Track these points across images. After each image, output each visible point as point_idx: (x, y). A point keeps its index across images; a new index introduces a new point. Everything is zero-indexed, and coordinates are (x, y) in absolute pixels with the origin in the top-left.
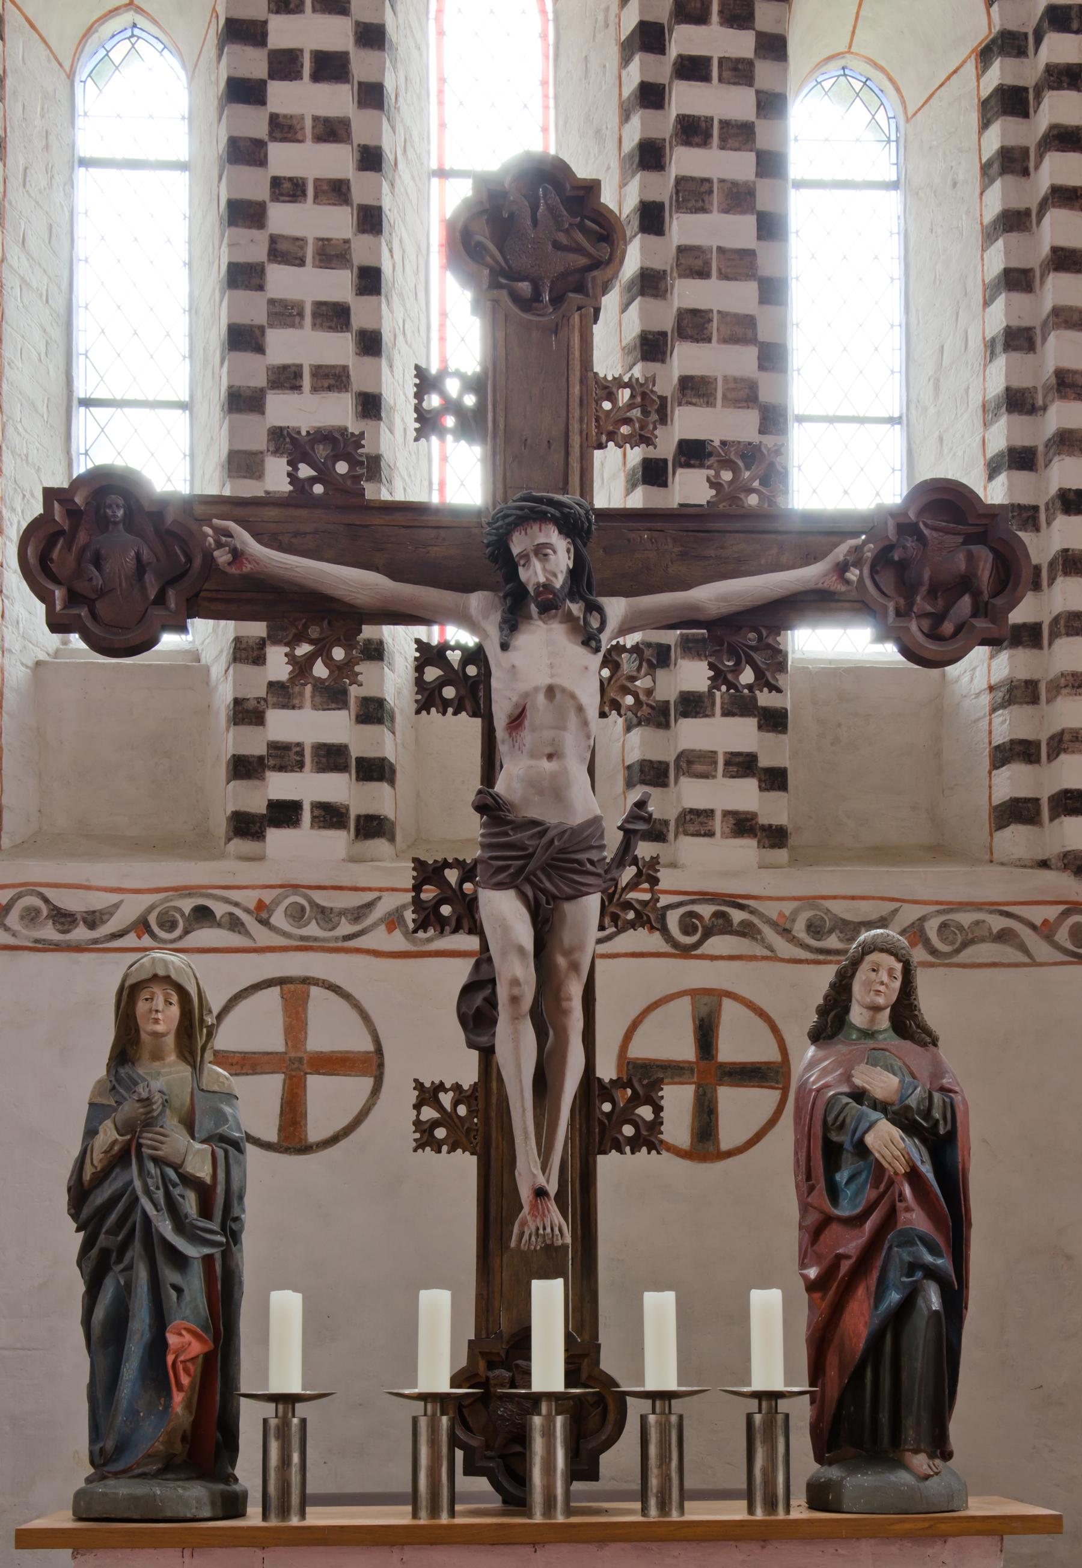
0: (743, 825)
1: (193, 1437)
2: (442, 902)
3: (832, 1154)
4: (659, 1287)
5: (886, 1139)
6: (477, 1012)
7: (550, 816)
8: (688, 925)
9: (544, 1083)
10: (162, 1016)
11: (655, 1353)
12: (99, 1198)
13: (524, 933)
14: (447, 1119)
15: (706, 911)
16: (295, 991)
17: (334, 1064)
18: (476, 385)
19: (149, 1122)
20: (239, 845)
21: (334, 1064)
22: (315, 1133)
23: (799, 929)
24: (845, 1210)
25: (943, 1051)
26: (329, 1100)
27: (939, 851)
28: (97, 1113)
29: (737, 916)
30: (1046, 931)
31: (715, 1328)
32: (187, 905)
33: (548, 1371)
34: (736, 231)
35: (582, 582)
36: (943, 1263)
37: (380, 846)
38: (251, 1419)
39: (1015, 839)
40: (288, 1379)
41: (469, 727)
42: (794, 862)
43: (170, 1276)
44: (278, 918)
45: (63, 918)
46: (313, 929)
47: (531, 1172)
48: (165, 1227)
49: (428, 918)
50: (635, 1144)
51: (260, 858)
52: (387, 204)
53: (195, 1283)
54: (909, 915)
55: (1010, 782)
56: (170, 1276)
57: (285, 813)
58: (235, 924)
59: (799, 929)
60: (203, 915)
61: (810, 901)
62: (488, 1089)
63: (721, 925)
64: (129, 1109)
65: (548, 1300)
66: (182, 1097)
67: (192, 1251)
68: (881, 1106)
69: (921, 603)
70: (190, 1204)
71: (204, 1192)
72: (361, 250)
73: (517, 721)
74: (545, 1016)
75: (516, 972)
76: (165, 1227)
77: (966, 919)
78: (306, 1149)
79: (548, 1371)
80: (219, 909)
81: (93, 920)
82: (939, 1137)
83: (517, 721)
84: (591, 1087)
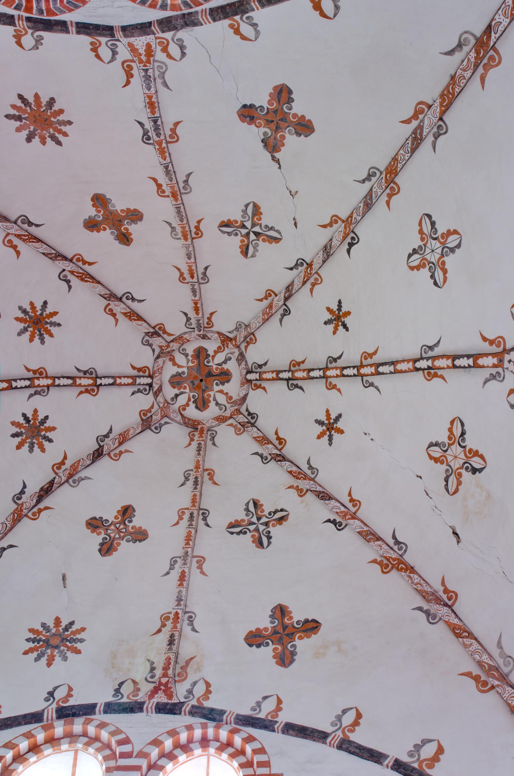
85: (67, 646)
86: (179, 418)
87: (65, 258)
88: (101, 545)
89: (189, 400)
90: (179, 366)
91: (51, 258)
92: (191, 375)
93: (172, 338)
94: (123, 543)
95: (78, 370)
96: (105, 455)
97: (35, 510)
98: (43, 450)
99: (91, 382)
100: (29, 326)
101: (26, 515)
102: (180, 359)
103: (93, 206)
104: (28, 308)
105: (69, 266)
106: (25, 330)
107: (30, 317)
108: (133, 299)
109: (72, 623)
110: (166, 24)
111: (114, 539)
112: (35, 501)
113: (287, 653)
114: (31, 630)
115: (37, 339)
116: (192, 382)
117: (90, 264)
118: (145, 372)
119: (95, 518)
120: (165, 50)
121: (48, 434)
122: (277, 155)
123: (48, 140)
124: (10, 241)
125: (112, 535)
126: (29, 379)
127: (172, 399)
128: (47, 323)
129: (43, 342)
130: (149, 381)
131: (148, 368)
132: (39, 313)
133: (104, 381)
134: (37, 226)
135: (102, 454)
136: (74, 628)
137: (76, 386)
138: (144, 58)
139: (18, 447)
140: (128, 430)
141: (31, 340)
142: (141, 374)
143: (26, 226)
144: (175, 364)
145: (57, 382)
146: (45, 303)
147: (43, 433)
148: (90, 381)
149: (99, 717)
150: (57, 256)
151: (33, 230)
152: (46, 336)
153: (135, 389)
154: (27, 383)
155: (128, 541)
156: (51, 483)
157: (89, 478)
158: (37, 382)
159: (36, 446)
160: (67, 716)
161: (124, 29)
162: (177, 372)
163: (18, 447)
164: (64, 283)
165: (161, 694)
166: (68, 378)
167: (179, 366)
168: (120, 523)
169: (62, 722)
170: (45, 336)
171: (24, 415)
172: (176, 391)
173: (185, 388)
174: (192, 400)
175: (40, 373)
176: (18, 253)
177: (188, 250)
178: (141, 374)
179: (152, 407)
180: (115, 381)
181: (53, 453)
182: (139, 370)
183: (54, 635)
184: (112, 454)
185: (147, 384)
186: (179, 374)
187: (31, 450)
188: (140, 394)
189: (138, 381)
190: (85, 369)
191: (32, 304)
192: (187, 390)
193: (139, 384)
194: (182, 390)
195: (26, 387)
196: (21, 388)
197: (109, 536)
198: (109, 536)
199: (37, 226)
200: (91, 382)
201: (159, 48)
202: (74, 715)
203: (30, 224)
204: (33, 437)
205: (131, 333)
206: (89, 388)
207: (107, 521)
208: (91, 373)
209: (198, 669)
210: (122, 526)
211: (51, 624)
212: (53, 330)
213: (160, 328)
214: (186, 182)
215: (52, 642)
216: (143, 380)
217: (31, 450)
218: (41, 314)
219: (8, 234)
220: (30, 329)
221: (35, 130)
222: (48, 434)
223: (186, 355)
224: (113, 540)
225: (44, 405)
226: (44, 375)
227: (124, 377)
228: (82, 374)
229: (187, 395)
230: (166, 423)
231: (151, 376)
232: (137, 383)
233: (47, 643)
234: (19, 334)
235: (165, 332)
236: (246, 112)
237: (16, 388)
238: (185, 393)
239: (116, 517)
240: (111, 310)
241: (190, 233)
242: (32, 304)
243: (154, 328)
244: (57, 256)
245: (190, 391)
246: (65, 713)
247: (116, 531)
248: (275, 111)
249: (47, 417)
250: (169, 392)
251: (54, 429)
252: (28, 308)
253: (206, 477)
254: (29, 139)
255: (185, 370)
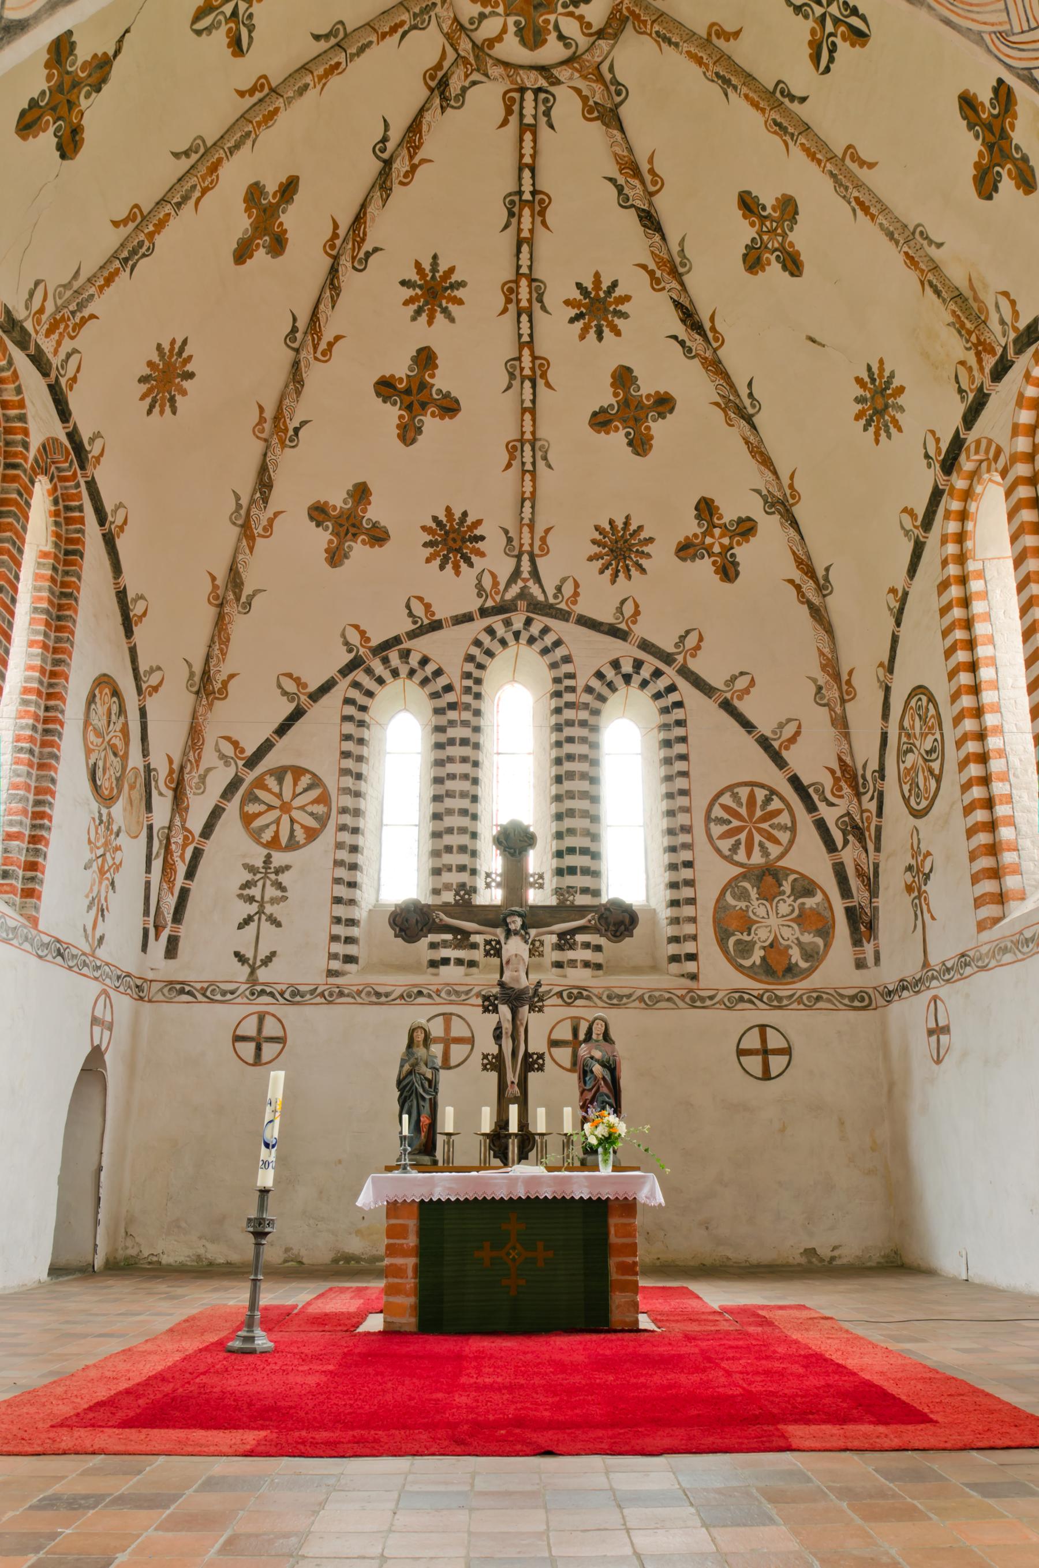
0: (587, 964)
1: (426, 1145)
2: (489, 1005)
3: (585, 1073)
4: (486, 1105)
5: (597, 1069)
6: (498, 1036)
7: (516, 986)
8: (570, 996)
9: (514, 1054)
10: (420, 1036)
11: (540, 1123)
12: (404, 1083)
13: (509, 1016)
14: (490, 1063)
15: (575, 991)
16: (447, 1017)
17: (459, 1040)
18: (500, 875)
19: (417, 1064)
20: (432, 970)
21: (459, 1040)
22: (453, 1063)
23: (604, 997)
24: (588, 1087)
25: (617, 1046)
26: (458, 1052)
27: (654, 969)
28: (403, 1062)
29: (585, 993)
30: (682, 998)
31: (554, 1117)
32: (415, 990)
33: (513, 1127)
34: (584, 785)
35: (524, 926)
36: (612, 1101)
37: (474, 970)
38: (440, 1140)
39: (674, 967)
40: (449, 1128)
41: (497, 960)
42: (605, 974)
43: (422, 1103)
44: (443, 994)
45: (378, 994)
46: (453, 998)
47: (511, 1077)
48: (421, 1091)
49: (486, 1010)
50: (538, 1070)
51: (437, 975)
52: (478, 848)
53: (427, 1105)
54: (639, 992)
55: (673, 949)
56: (422, 1103)
57: (445, 961)
58: (430, 996)
59: (604, 997)
60: (420, 993)
61: (608, 988)
62: (500, 1057)
63: (580, 996)
64: (412, 1060)
65: (513, 1110)
66: (425, 1057)
67: (427, 1097)
68: (597, 1061)
69: (612, 928)
70: (426, 1084)
71: (430, 1082)
72: (475, 689)
73: (508, 962)
74: (514, 1037)
75: (507, 1026)
76: (421, 1091)
77: (657, 994)
78: (450, 1068)
79: (513, 1127)
80: (425, 991)
81: (387, 995)
82: (611, 1067)
83: (508, 962)
84: (527, 1055)
85: (890, 396)
86: (603, 44)
87: (334, 271)
88: (785, 268)
89: (571, 14)
90: (504, 30)
91: (338, 295)
92: (522, 9)
93: (449, 50)
94: (792, 237)
95: (506, 227)
96: (651, 204)
97: (710, 335)
98: (627, 298)
99: (527, 212)
100: (440, 306)
101: (715, 350)
102: (490, 28)
103: (251, 257)
104: (413, 307)
105: (345, 261)
106: (445, 311)
107: (426, 303)
108: (385, 140)
109: (869, 368)
110: (23, 343)
111: (782, 244)
112: (697, 337)
113: (1020, 164)
114: (857, 418)
115: (459, 293)
116: (536, 7)
117: (336, 226)
118: (513, 99)
119: (745, 256)
120: (41, 310)
121: (604, 287)
122: (111, 53)
123: (185, 355)
124: (324, 354)
125: (776, 245)
126: (519, 315)
127: (567, 46)
128: (433, 277)
129: (462, 284)
130: (529, 96)
131: (506, 93)
132: (418, 291)
133: (527, 187)
134: (295, 319)
135: (648, 212)
136: (875, 369)
137: (532, 238)
138: (62, 326)
139: (618, 333)
140: (616, 155)
141: (460, 302)
142: (516, 107)
143: (299, 335)
144: (499, 38)
145: (524, 270)
146: (403, 283)
147: (602, 295)
148: (527, 204)
149: (971, 437)
150: (332, 281)
151: (301, 325)
152: (454, 278)
153: (536, 306)
154: (524, 318)
155: (791, 229)
156: (677, 305)
157: (683, 239)
158: (524, 304)
159: (620, 307)
160: (952, 465)
161: (45, 374)
162: (516, 34)
163: (618, 333)
164: (371, 260)
165: (985, 357)
166: (519, 251)
167: (504, 30)
168: (762, 224)
169: (954, 474)
170: (453, 280)
171: (572, 321)
172: (552, 37)
173: (547, 21)
174: (571, 8)
175: (510, 292)
176: (338, 338)
177: (293, 98)
178: (516, 107)
179: (578, 91)
180: (527, 165)
181: (634, 284)
182: (509, 111)
183: (873, 398)
184: (652, 189)
185: (530, 286)
186: (520, 32)
187: (624, 315)
188: (553, 113)
189: (529, 120)
190: (505, 213)
191: (406, 303)
192: (552, 18)
193: (535, 117)
194: (551, 27)
195: (530, 321)
196: (531, 328)
197: (776, 250)
198: (776, 250)
199: (295, 319)
200: (527, 212)
201: (44, 317)
202: (956, 458)
203: (294, 330)
204: (606, 310)
205: (444, 131)
206: (537, 208)
207: (753, 240)
208: (512, 202)
209: (986, 286)
210: (768, 223)
211: (859, 392)
212: (443, 267)
213: (432, 78)
214: (187, 154)
215: (879, 407)
216: (526, 111)
217: (624, 315)
218: (421, 287)
219: (316, 359)
220: (444, 303)
221: (179, 376)
222: (604, 287)
223: (482, 16)
224: (782, 249)
225: (560, 290)
226: (513, 285)
227: (521, 148)
228: (514, 221)
229: (560, 18)
230: (611, 69)
231: (522, 90)
232: (532, 121)
233: (880, 412)
234: (452, 320)
235: (439, 66)
236: (68, 150)
237: (531, 336)
238: (556, 21)
239: (753, 224)
240: (406, 176)
241: (265, 99)
242: (406, 303)
243: (432, 90)
244: (332, 281)
245: (554, 11)
246: (949, 465)
247: (771, 238)
248: (54, 109)
249: (579, 286)
250: (552, 51)
251: (597, 276)
252: (413, 307)
253: (720, 43)
254: (190, 376)
255: (511, 20)
